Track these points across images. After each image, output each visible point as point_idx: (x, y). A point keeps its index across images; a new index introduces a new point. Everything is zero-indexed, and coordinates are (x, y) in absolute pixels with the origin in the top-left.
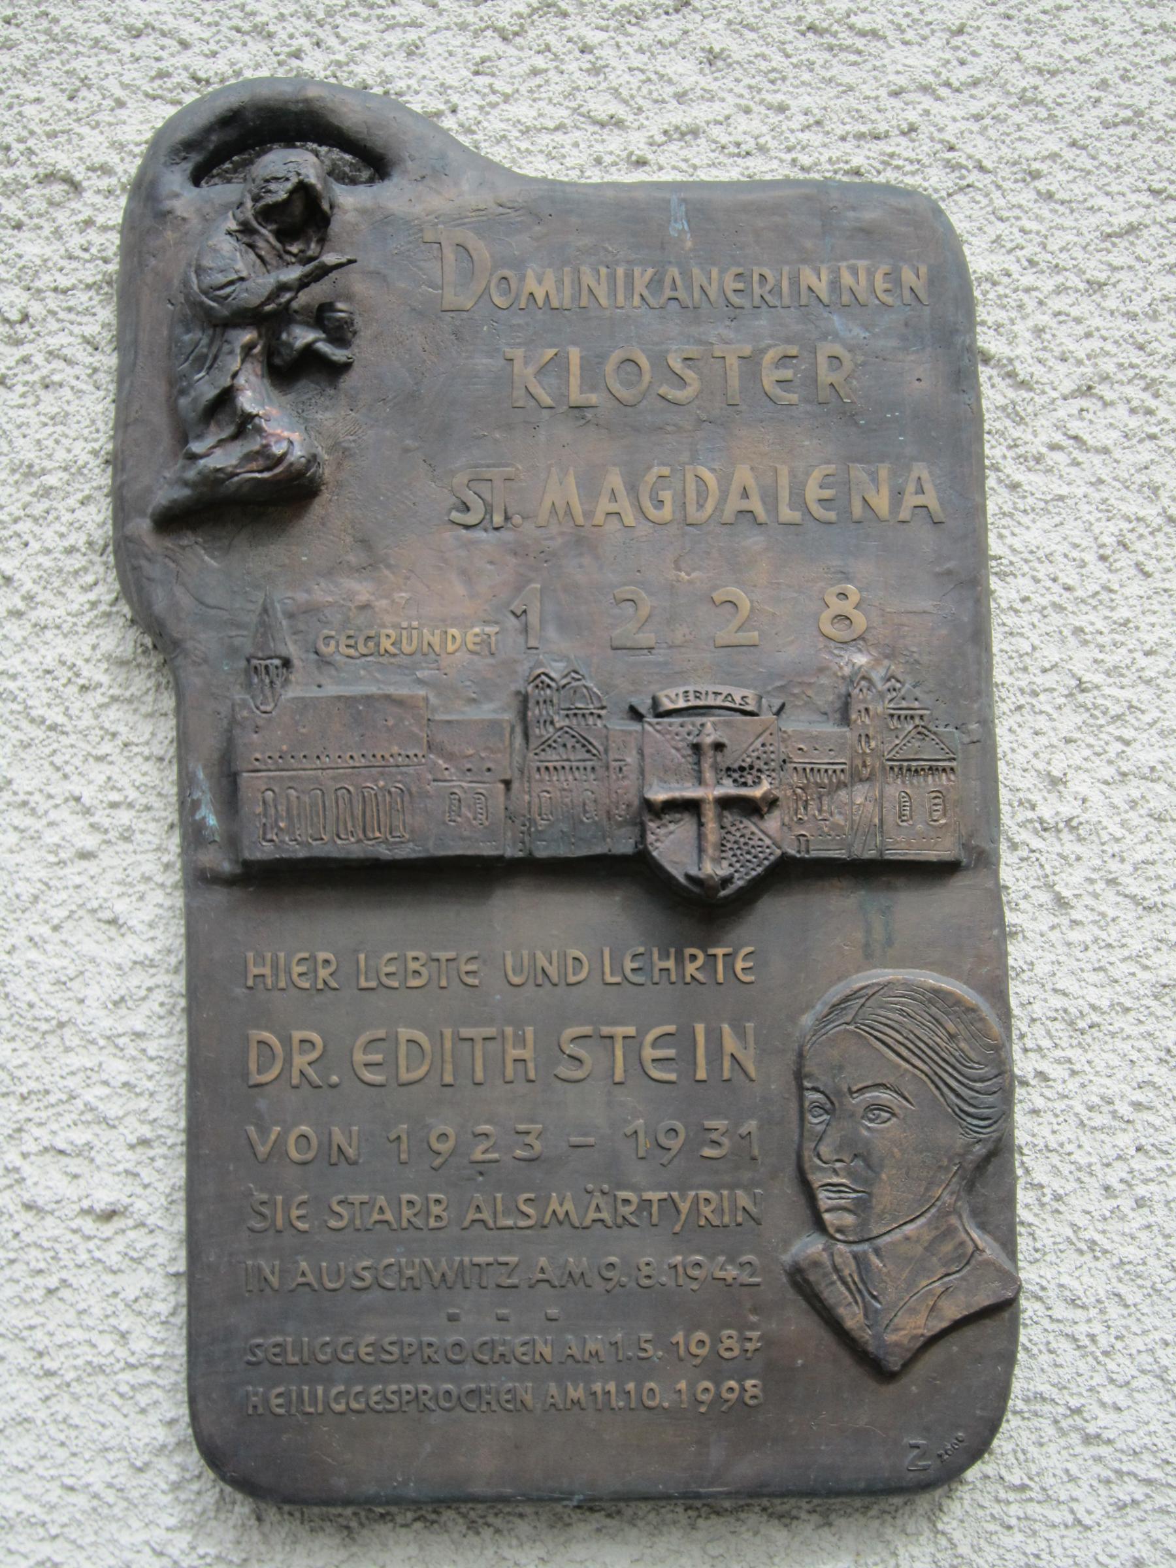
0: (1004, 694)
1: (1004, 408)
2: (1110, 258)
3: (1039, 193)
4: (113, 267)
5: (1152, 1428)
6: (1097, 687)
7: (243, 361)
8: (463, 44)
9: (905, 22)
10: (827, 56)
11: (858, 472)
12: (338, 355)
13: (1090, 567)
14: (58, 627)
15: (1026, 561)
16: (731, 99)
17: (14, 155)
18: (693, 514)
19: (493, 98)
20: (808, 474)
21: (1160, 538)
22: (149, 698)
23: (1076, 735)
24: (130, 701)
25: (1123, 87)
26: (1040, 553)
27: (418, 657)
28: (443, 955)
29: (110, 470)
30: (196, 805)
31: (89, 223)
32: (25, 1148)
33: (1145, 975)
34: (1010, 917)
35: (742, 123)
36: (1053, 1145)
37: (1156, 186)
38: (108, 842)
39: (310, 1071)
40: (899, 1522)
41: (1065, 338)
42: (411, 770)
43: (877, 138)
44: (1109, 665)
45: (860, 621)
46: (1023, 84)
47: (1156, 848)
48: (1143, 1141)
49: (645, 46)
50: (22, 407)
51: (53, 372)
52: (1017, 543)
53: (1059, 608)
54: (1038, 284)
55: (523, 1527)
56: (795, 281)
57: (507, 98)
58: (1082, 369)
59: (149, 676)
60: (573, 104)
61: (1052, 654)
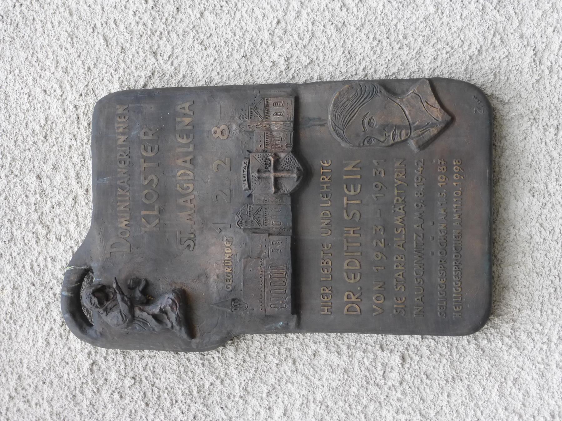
0: (247, 81)
1: (160, 80)
2: (114, 46)
3: (94, 68)
4: (119, 351)
5: (477, 33)
6: (245, 51)
7: (145, 311)
8: (52, 244)
9: (43, 109)
10: (54, 133)
11: (179, 127)
12: (143, 283)
13: (209, 53)
14: (226, 369)
15: (207, 73)
16: (68, 163)
17: (85, 381)
18: (191, 177)
19: (68, 235)
20: (179, 142)
21: (200, 31)
22: (247, 342)
23: (260, 58)
24: (248, 348)
25: (61, 40)
26: (204, 69)
27: (232, 260)
28: (322, 254)
29: (179, 353)
30: (276, 328)
31: (105, 358)
32: (383, 384)
33: (334, 37)
34: (315, 80)
35: (75, 159)
36: (386, 66)
37: (92, 30)
38: (290, 356)
39: (356, 296)
40: (505, 114)
41: (139, 60)
42: (265, 263)
43: (78, 118)
44: (238, 47)
45: (223, 127)
46: (61, 72)
47: (295, 33)
48: (385, 37)
49: (52, 189)
50: (160, 379)
51: (150, 369)
52: (201, 76)
53: (221, 63)
54: (122, 68)
55: (504, 233)
56: (122, 146)
57: (68, 231)
58: (148, 55)
59: (241, 342)
60: (70, 211)
61: (235, 65)
